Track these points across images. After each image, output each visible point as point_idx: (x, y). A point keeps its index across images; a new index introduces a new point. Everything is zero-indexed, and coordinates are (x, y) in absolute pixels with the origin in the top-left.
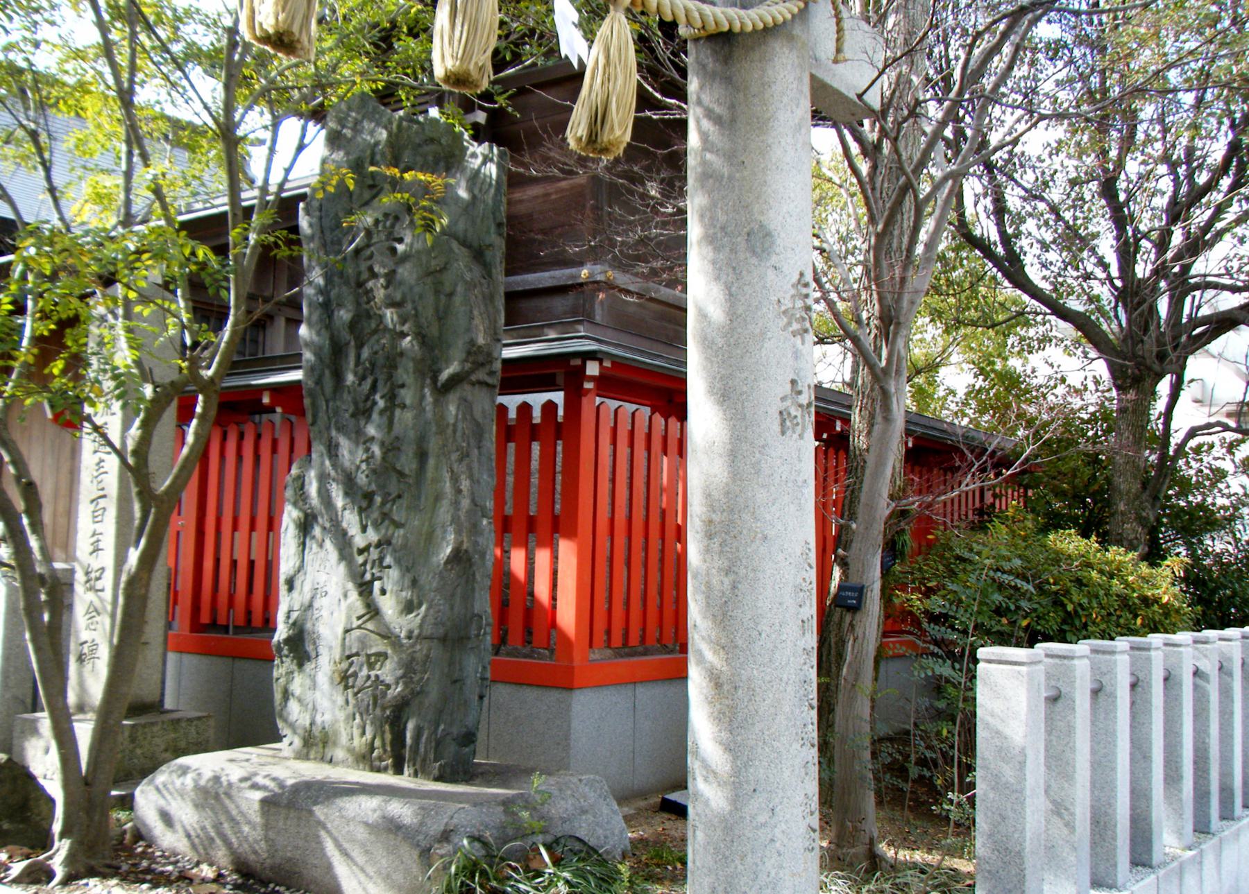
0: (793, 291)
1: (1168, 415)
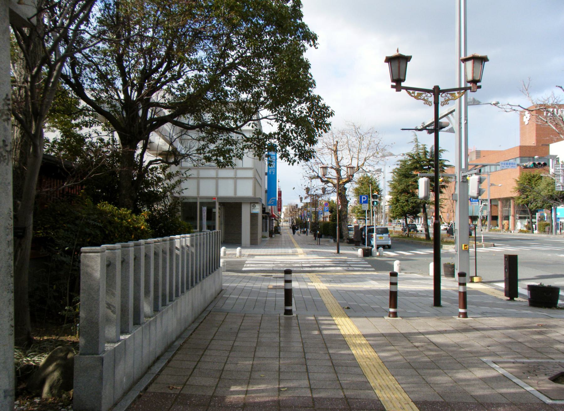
0: (3, 102)
1: (142, 155)
